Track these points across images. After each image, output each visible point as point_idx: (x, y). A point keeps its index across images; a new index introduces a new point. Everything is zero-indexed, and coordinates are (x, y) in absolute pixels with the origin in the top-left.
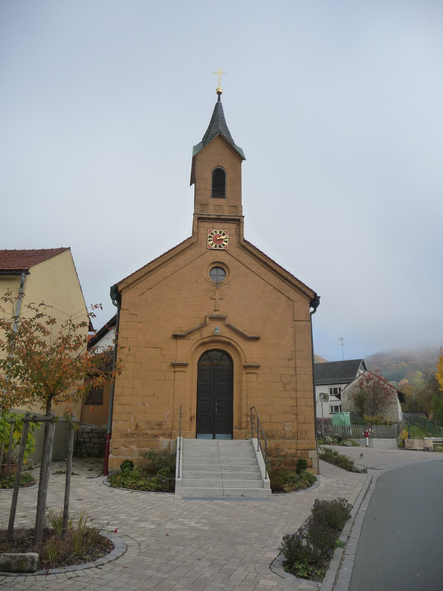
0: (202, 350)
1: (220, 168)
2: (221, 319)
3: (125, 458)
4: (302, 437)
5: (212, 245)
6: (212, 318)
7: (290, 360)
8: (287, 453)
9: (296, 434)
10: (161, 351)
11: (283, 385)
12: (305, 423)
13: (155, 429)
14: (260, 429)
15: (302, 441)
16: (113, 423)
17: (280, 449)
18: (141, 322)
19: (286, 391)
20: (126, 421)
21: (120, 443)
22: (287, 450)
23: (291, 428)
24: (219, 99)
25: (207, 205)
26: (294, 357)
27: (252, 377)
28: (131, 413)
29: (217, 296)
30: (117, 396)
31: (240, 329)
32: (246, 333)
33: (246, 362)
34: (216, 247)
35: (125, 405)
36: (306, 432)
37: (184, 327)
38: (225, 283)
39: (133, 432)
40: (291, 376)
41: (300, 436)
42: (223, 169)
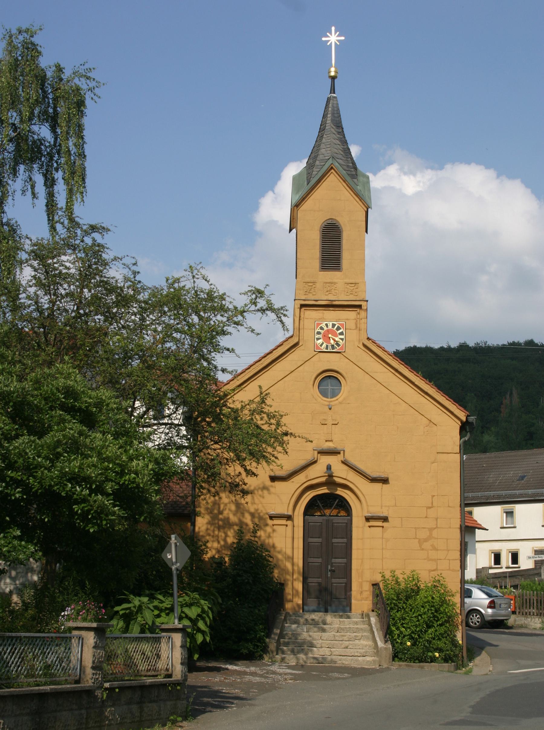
2: (334, 452)
6: (323, 452)
11: (419, 542)
19: (423, 549)
24: (333, 90)
29: (330, 422)
34: (327, 348)
40: (431, 530)
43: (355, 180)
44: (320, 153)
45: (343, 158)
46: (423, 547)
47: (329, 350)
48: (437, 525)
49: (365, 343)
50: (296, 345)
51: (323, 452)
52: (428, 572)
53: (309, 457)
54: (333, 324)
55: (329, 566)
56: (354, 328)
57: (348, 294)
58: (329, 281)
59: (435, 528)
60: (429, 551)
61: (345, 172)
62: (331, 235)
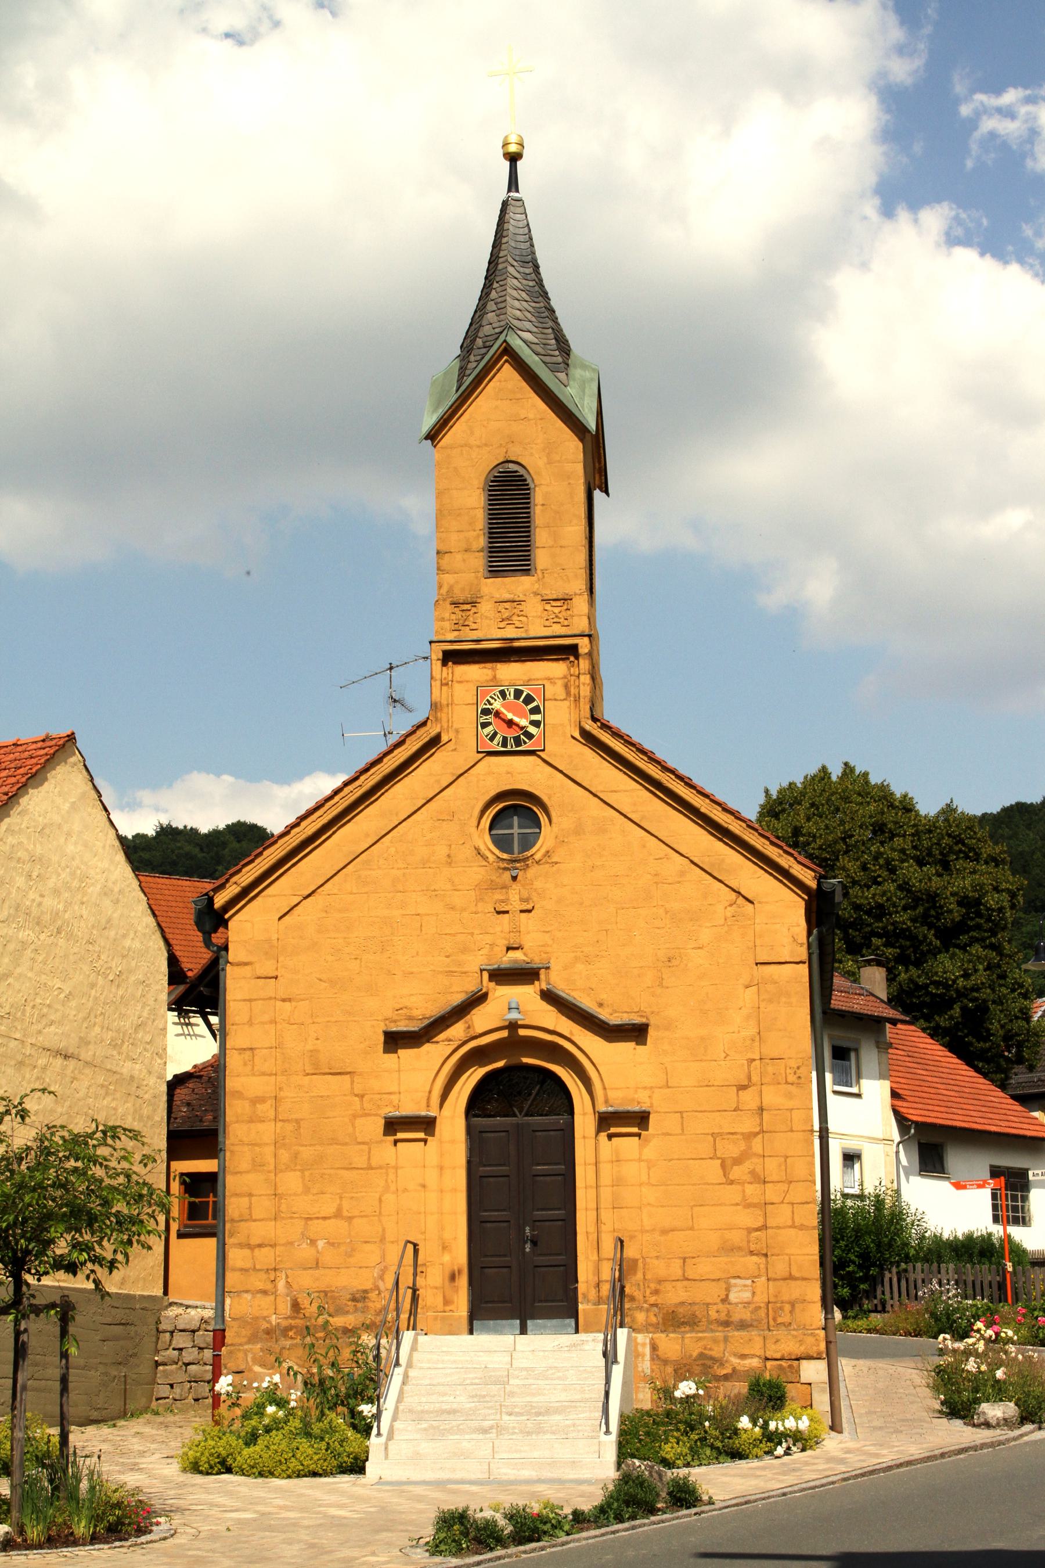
0: (474, 1076)
1: (512, 467)
2: (524, 975)
3: (488, 1436)
4: (780, 1320)
5: (492, 739)
6: (503, 976)
7: (742, 1088)
8: (734, 1370)
9: (762, 1313)
10: (352, 1082)
11: (723, 1165)
12: (791, 1277)
13: (347, 1312)
14: (64, 1361)
15: (781, 1333)
16: (228, 1301)
17: (712, 1358)
18: (290, 1000)
19: (732, 1182)
20: (265, 1292)
21: (250, 1356)
22: (735, 1361)
23: (747, 1295)
24: (513, 183)
25: (473, 603)
26: (755, 1078)
27: (628, 1146)
28: (275, 1270)
29: (515, 905)
30: (233, 1220)
31: (587, 1003)
32: (604, 1015)
33: (606, 1101)
34: (504, 743)
35: (260, 1246)
36: (793, 1305)
37: (423, 1004)
38: (537, 857)
39: (285, 1323)
40: (749, 1136)
41: (775, 1320)
42: (522, 471)
43: (562, 376)
44: (484, 322)
45: (535, 330)
46: (731, 1177)
47: (509, 748)
48: (761, 1124)
49: (588, 728)
50: (435, 742)
51: (503, 976)
52: (745, 1232)
53: (469, 985)
54: (516, 691)
55: (527, 1228)
56: (563, 696)
57: (547, 623)
58: (507, 596)
59: (758, 1133)
60: (746, 1185)
61: (537, 358)
62: (509, 496)
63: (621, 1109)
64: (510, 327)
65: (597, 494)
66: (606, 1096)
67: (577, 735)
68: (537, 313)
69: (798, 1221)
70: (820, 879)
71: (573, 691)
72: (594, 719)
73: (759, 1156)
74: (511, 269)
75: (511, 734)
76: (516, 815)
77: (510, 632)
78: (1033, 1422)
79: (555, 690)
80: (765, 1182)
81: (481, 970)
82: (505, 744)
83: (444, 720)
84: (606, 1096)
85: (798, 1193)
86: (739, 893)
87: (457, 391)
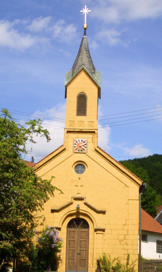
0: (69, 219)
2: (81, 199)
5: (76, 150)
6: (76, 199)
7: (124, 225)
19: (121, 244)
26: (127, 223)
27: (100, 236)
33: (96, 227)
40: (125, 235)
43: (94, 75)
44: (78, 62)
46: (121, 243)
49: (96, 149)
50: (64, 149)
51: (76, 199)
53: (69, 201)
56: (91, 142)
63: (99, 228)
64: (84, 64)
65: (99, 99)
66: (96, 225)
67: (94, 150)
68: (89, 61)
69: (134, 253)
70: (143, 183)
71: (93, 141)
72: (98, 147)
73: (127, 239)
74: (84, 52)
75: (80, 149)
76: (80, 166)
77: (81, 128)
78: (79, 212)
79: (90, 140)
80: (128, 245)
81: (72, 198)
82: (79, 151)
83: (66, 145)
84: (96, 225)
85: (135, 247)
86: (126, 185)
87: (72, 76)
